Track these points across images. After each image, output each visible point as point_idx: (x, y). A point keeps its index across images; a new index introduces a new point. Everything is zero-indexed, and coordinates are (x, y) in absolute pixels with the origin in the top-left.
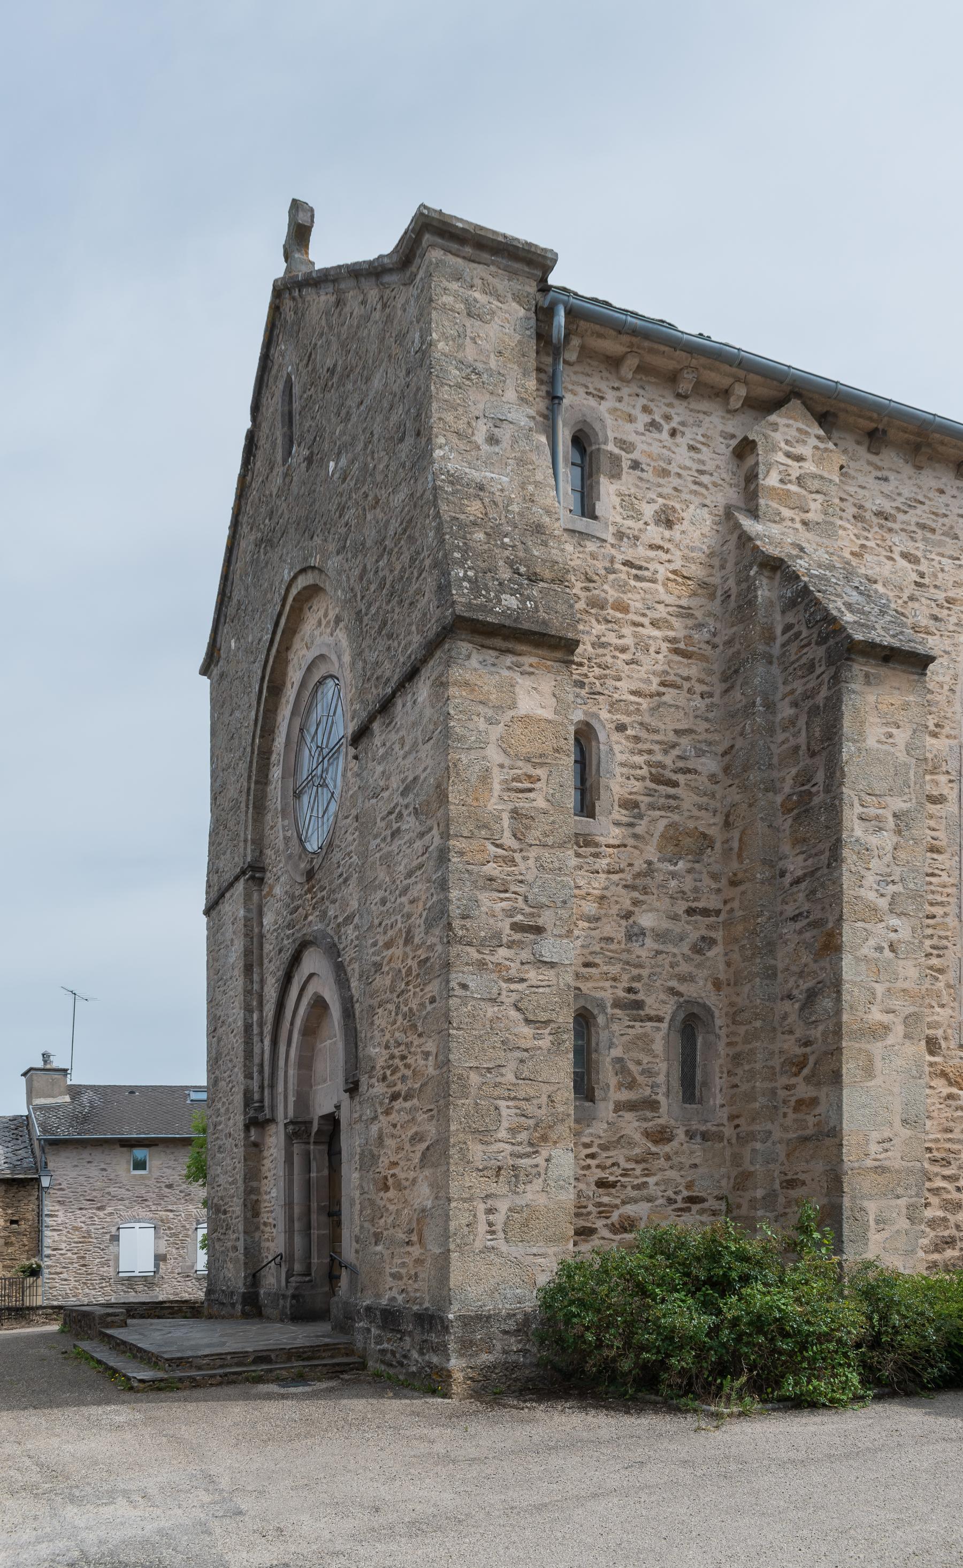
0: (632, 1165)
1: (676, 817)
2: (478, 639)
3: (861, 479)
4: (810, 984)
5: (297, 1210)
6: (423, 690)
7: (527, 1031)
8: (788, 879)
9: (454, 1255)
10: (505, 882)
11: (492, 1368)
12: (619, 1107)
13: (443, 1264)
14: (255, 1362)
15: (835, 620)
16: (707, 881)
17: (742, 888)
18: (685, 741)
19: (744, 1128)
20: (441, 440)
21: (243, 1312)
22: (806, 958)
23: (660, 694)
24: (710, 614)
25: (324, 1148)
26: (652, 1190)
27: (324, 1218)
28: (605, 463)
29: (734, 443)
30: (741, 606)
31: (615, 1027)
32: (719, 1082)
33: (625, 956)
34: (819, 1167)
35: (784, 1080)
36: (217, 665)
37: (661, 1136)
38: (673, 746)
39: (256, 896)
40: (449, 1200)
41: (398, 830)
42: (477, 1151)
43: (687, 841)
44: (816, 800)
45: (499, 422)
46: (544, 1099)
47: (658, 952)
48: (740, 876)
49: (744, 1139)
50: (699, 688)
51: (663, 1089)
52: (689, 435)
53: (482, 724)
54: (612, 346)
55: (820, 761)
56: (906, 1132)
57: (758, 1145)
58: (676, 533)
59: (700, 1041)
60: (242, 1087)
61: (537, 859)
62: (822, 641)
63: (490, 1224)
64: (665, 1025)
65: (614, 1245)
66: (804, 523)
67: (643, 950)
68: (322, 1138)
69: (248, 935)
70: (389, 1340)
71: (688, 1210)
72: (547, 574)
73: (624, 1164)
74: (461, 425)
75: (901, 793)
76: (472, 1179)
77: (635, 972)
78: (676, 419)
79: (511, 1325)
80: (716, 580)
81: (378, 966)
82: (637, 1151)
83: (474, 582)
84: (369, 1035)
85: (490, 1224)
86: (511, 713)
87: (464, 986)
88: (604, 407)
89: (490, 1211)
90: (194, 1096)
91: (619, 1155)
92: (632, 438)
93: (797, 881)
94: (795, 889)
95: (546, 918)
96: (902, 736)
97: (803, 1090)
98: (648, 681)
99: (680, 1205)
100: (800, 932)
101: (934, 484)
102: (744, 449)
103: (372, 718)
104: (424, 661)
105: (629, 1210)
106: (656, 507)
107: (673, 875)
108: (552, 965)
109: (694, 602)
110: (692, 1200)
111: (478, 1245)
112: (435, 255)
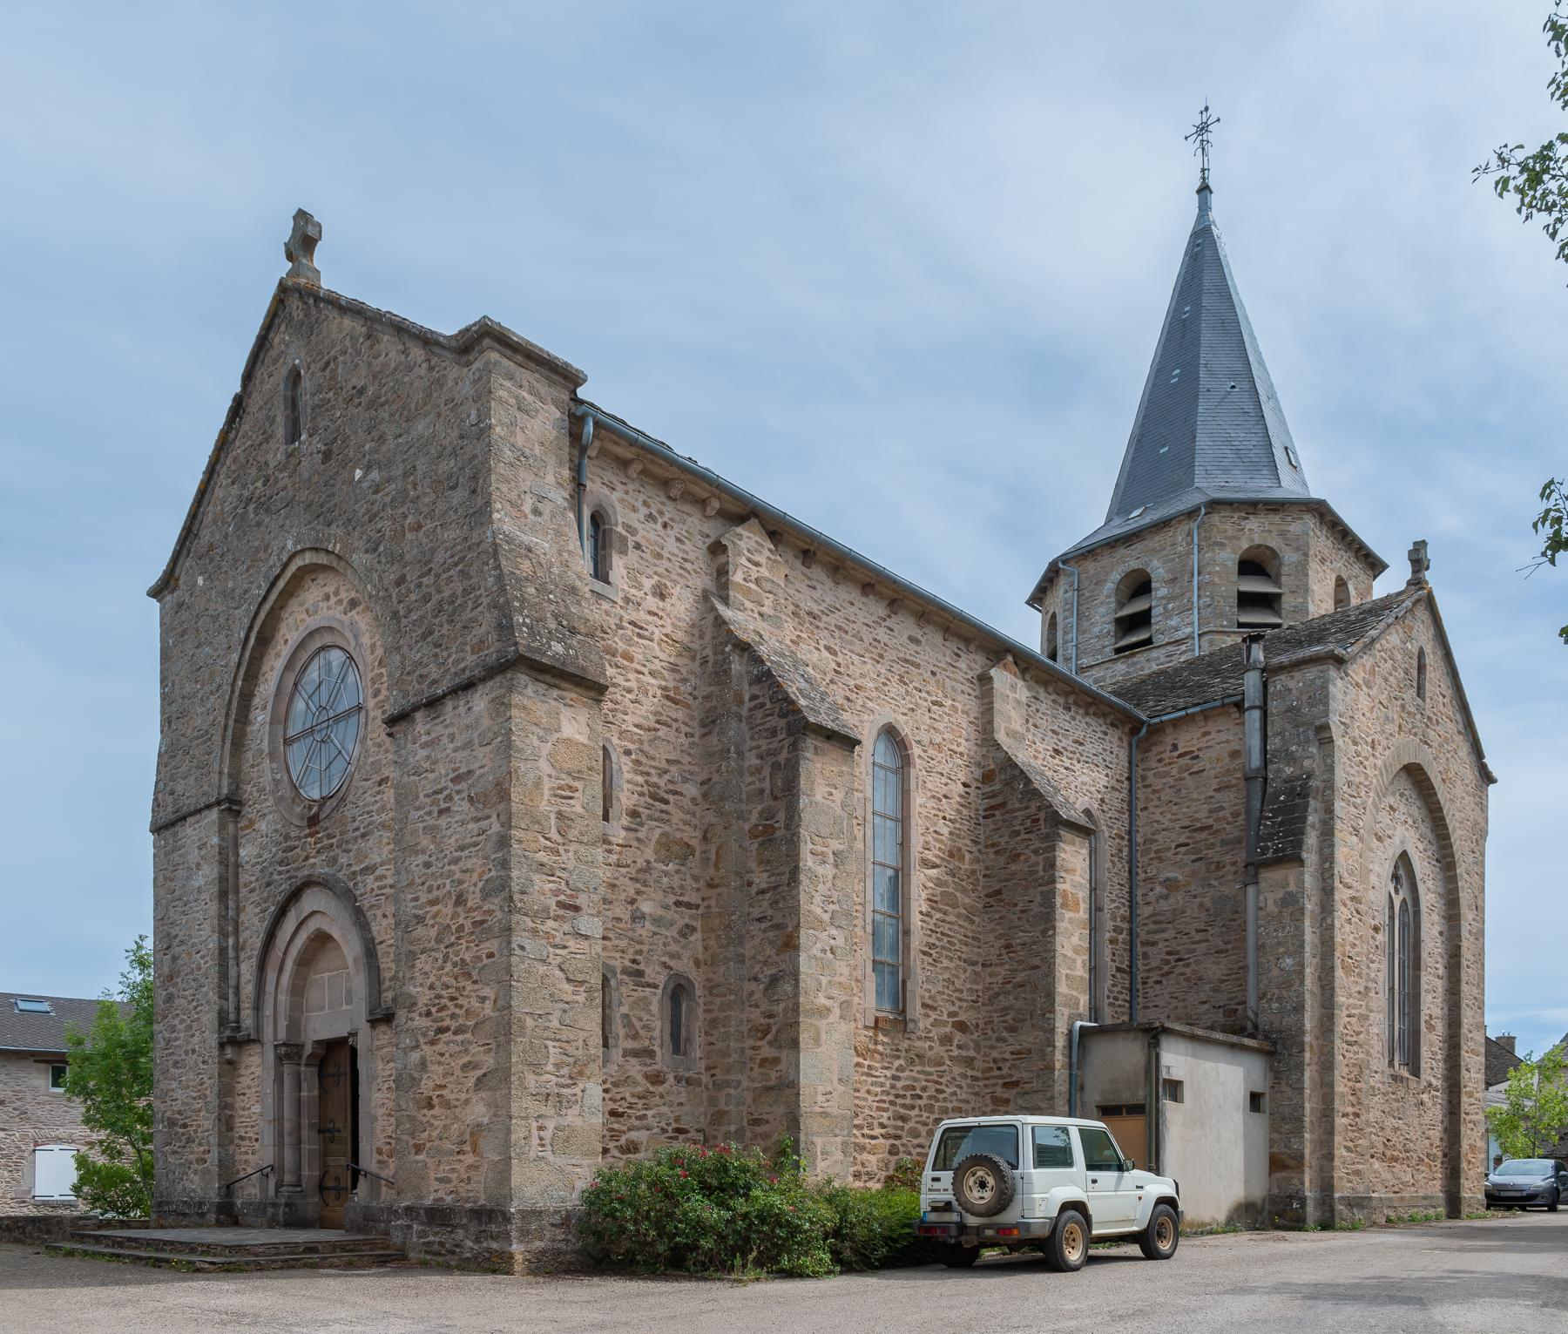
0: (635, 1100)
1: (667, 829)
2: (534, 674)
3: (798, 585)
4: (773, 971)
5: (287, 1126)
6: (480, 702)
7: (568, 987)
8: (754, 889)
9: (514, 1162)
10: (552, 868)
11: (544, 1252)
12: (627, 1053)
13: (503, 1170)
14: (304, 1252)
15: (793, 703)
16: (690, 881)
17: (719, 890)
18: (674, 769)
19: (720, 1077)
20: (498, 506)
21: (218, 1220)
22: (769, 951)
23: (656, 730)
24: (691, 672)
25: (315, 1070)
26: (650, 1121)
27: (314, 1135)
28: (616, 542)
29: (709, 541)
30: (720, 674)
31: (623, 989)
32: (698, 1040)
33: (630, 934)
34: (780, 1110)
35: (751, 1042)
36: (172, 592)
37: (657, 1079)
38: (666, 772)
39: (231, 827)
40: (510, 1117)
41: (448, 810)
42: (531, 1080)
43: (676, 849)
44: (778, 834)
45: (541, 499)
46: (580, 1043)
47: (655, 933)
48: (717, 881)
49: (718, 1086)
50: (684, 729)
51: (658, 1042)
52: (676, 529)
53: (536, 742)
54: (624, 452)
55: (781, 805)
56: (841, 1088)
57: (732, 1091)
58: (667, 604)
59: (684, 1006)
60: (216, 1007)
61: (576, 853)
62: (783, 715)
63: (541, 1139)
64: (659, 991)
65: (621, 1164)
66: (761, 615)
67: (645, 930)
68: (335, 1063)
69: (223, 862)
70: (436, 1234)
71: (676, 1138)
72: (583, 630)
73: (629, 1099)
74: (513, 495)
75: (838, 838)
76: (527, 1102)
77: (638, 947)
78: (667, 515)
79: (557, 1219)
80: (695, 646)
81: (420, 920)
82: (639, 1089)
83: (530, 628)
84: (408, 976)
85: (541, 1139)
86: (557, 735)
87: (522, 948)
88: (615, 496)
89: (541, 1128)
90: (22, 1005)
91: (626, 1091)
92: (635, 524)
93: (762, 892)
94: (760, 897)
95: (582, 900)
96: (839, 795)
97: (767, 1051)
98: (647, 718)
99: (670, 1134)
100: (765, 931)
101: (846, 596)
102: (717, 549)
103: (416, 708)
104: (483, 680)
105: (633, 1135)
106: (653, 582)
107: (666, 874)
108: (587, 937)
109: (680, 661)
110: (679, 1131)
111: (532, 1155)
112: (494, 356)
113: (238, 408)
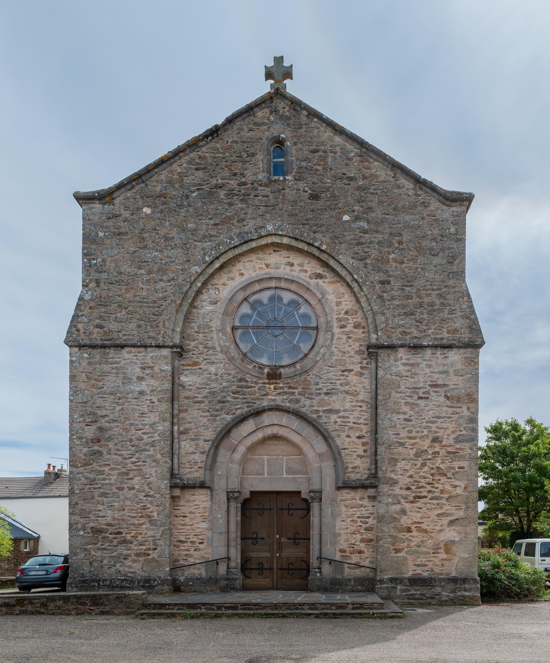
104: (459, 347)
113: (214, 133)
